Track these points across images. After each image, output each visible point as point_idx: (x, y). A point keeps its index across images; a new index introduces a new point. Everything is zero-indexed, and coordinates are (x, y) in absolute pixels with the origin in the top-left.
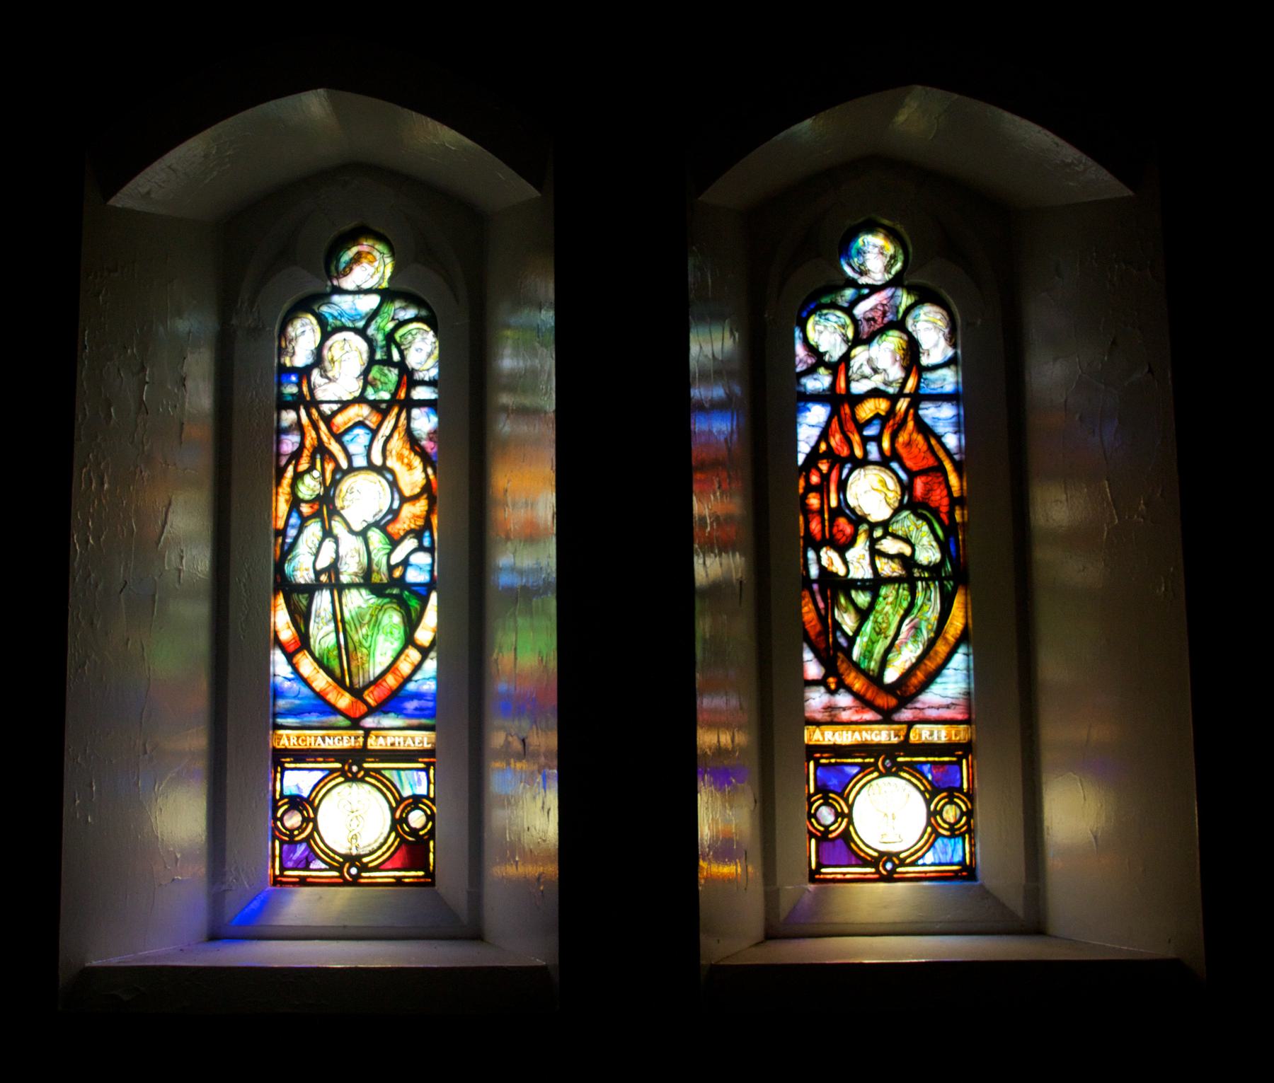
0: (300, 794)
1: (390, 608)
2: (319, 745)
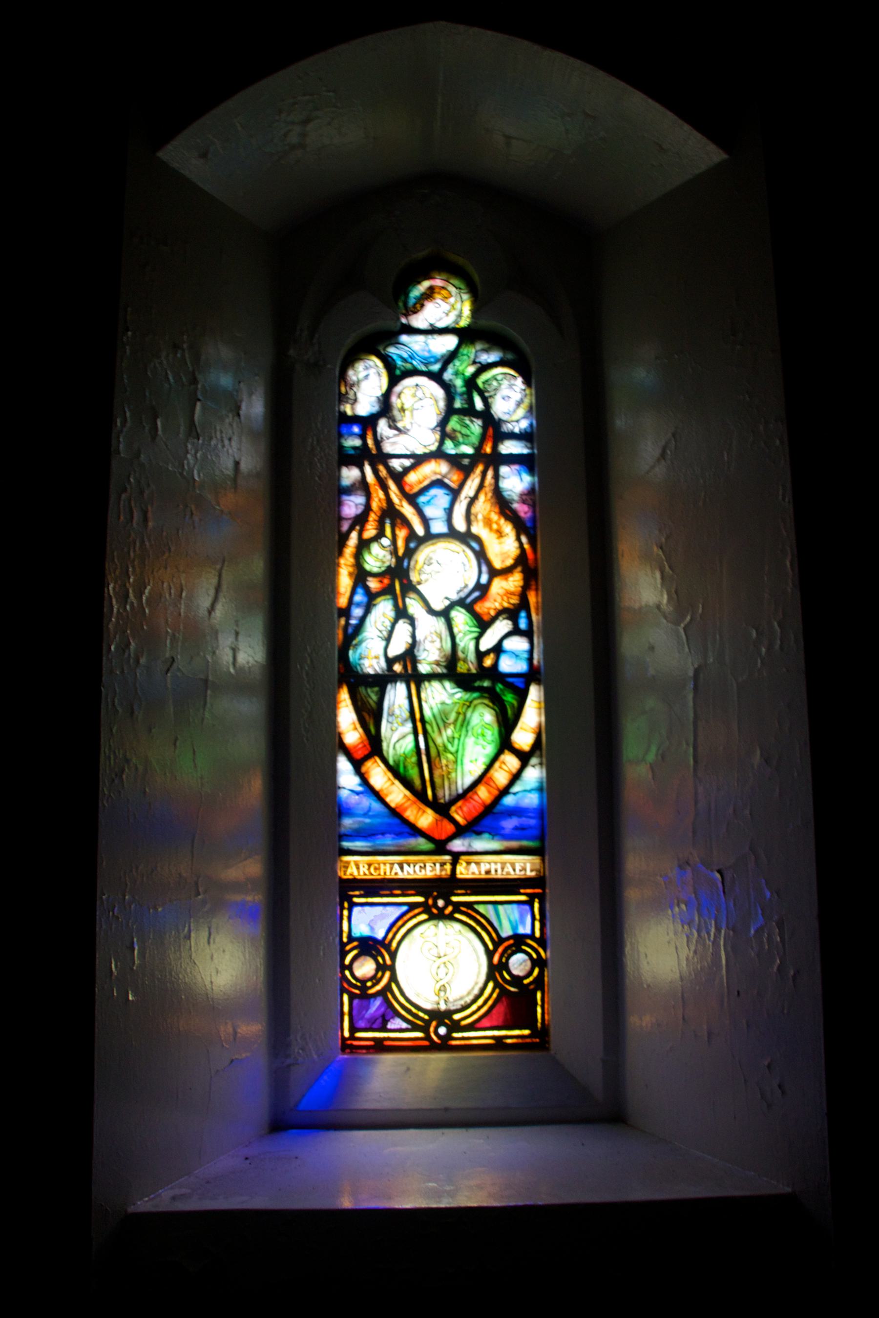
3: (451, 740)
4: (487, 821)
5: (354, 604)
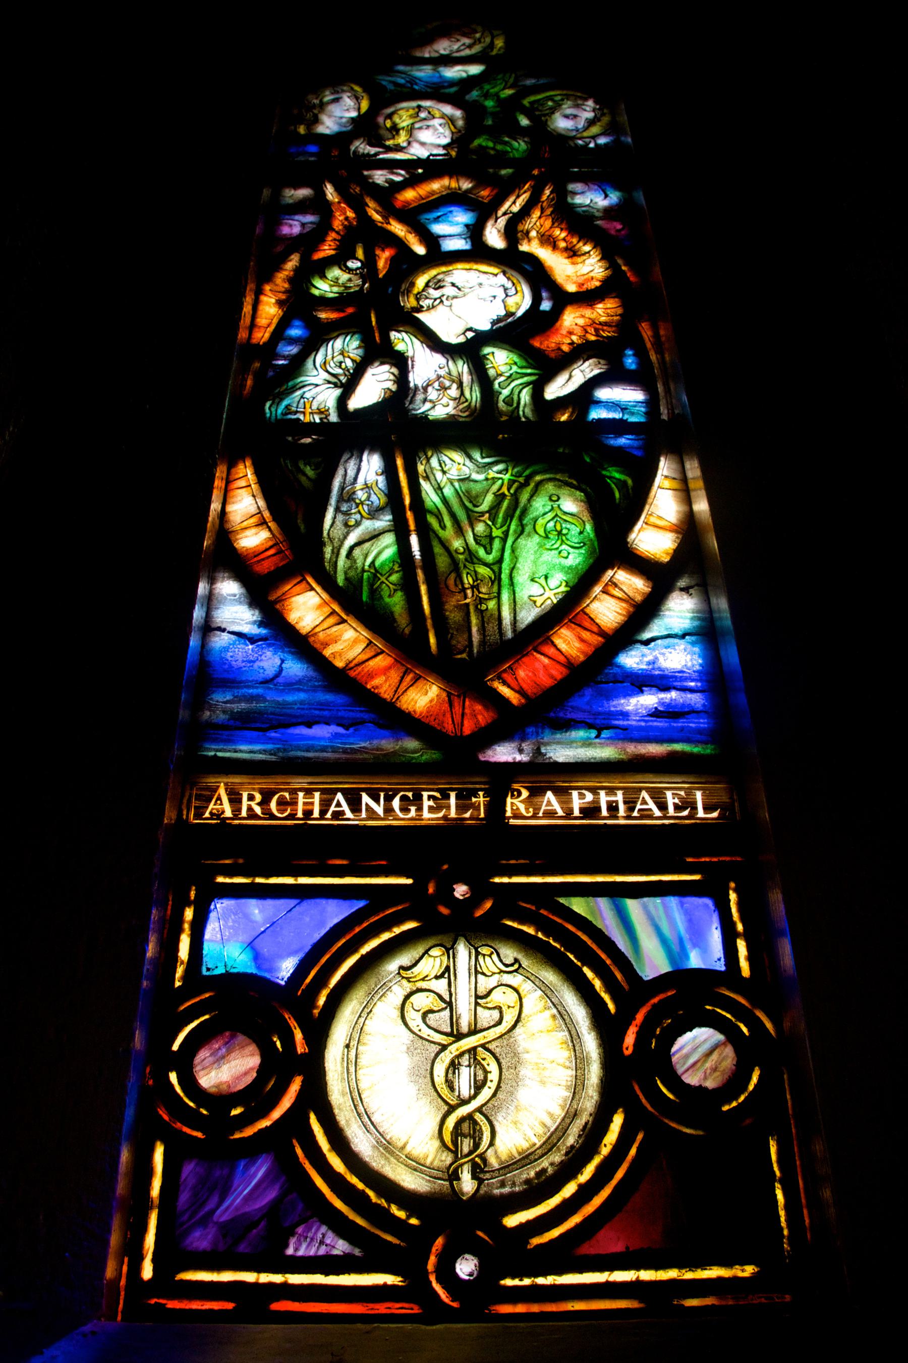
0: (256, 1070)
1: (550, 480)
2: (338, 815)
3: (487, 541)
4: (583, 700)
5: (285, 339)
